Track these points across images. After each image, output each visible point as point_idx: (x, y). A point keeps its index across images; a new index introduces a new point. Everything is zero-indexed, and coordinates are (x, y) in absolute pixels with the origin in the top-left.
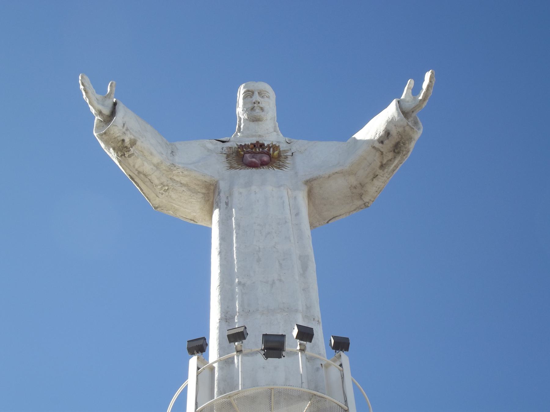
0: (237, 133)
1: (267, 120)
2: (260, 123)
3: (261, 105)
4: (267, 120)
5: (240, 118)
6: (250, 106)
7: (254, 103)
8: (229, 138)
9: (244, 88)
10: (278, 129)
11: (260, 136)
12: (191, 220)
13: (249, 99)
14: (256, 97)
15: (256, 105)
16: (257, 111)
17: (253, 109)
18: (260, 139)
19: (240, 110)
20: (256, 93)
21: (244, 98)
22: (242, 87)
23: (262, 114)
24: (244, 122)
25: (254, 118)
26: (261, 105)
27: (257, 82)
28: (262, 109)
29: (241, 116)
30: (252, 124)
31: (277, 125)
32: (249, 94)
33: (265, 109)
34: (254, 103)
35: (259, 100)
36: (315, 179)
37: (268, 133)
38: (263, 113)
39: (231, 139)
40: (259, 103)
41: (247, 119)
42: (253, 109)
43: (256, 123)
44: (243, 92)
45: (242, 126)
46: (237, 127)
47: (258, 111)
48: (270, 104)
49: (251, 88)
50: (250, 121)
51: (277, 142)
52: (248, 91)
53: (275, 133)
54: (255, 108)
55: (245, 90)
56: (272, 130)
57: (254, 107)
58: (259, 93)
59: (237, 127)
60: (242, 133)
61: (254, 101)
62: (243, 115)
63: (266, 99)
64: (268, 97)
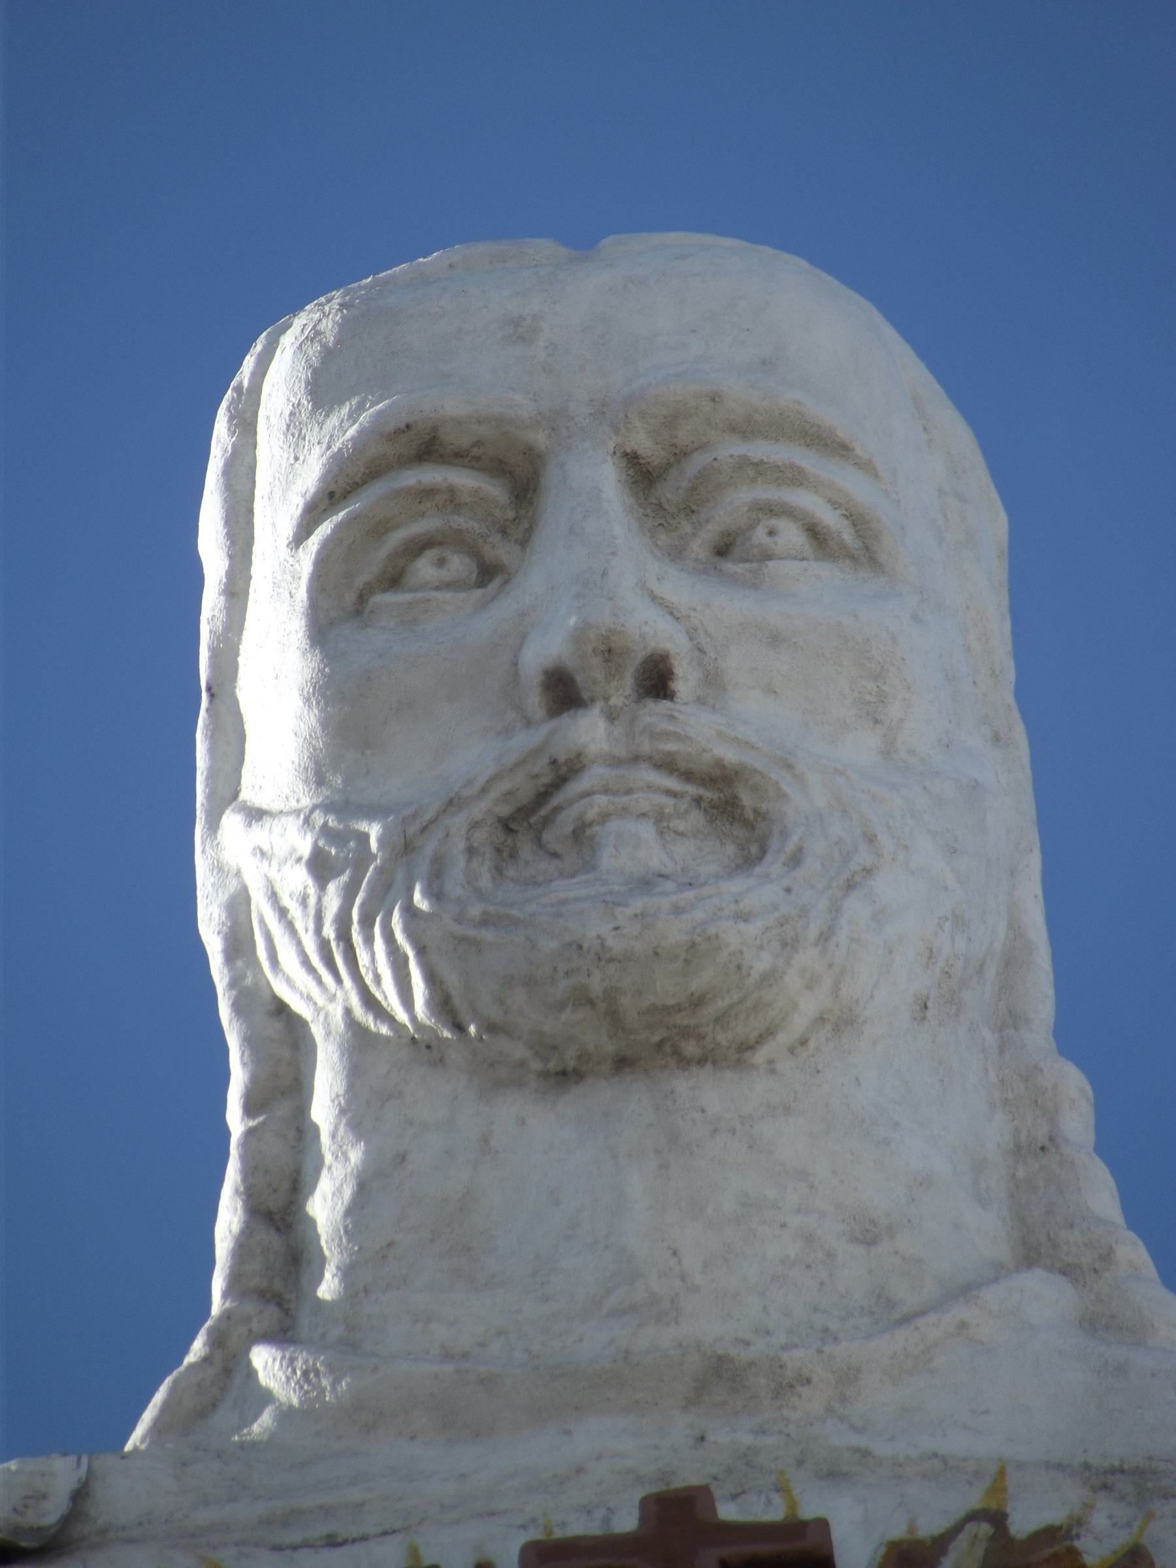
0: (228, 1362)
1: (842, 1022)
2: (707, 1094)
3: (691, 726)
4: (842, 1022)
5: (283, 1038)
6: (478, 754)
7: (563, 692)
8: (63, 1473)
9: (323, 389)
10: (1101, 1195)
11: (720, 1378)
12: (1167, 1461)
13: (452, 621)
14: (601, 569)
15: (590, 731)
16: (634, 845)
17: (534, 818)
18: (730, 1435)
19: (258, 854)
20: (590, 484)
21: (341, 608)
22: (280, 373)
23: (740, 913)
24: (359, 1112)
25: (570, 1007)
26: (691, 726)
27: (582, 238)
28: (730, 806)
29: (296, 986)
30: (543, 1136)
31: (1078, 1123)
32: (427, 516)
33: (802, 802)
34: (563, 692)
35: (651, 629)
36: (325, 510)
37: (888, 1313)
38: (761, 892)
39: (121, 1499)
40: (656, 680)
41: (422, 1047)
42: (534, 818)
43: (633, 1103)
44: (310, 475)
45: (325, 1206)
46: (229, 1219)
47: (641, 869)
48: (889, 687)
49: (478, 386)
50: (494, 1077)
51: (1103, 1479)
52: (424, 444)
53: (1044, 1296)
54: (585, 798)
55: (343, 428)
56: (985, 1232)
57: (565, 771)
58: (642, 475)
59: (229, 1219)
60: (342, 1340)
61: (546, 648)
62: (336, 954)
63: (810, 591)
64: (853, 546)
